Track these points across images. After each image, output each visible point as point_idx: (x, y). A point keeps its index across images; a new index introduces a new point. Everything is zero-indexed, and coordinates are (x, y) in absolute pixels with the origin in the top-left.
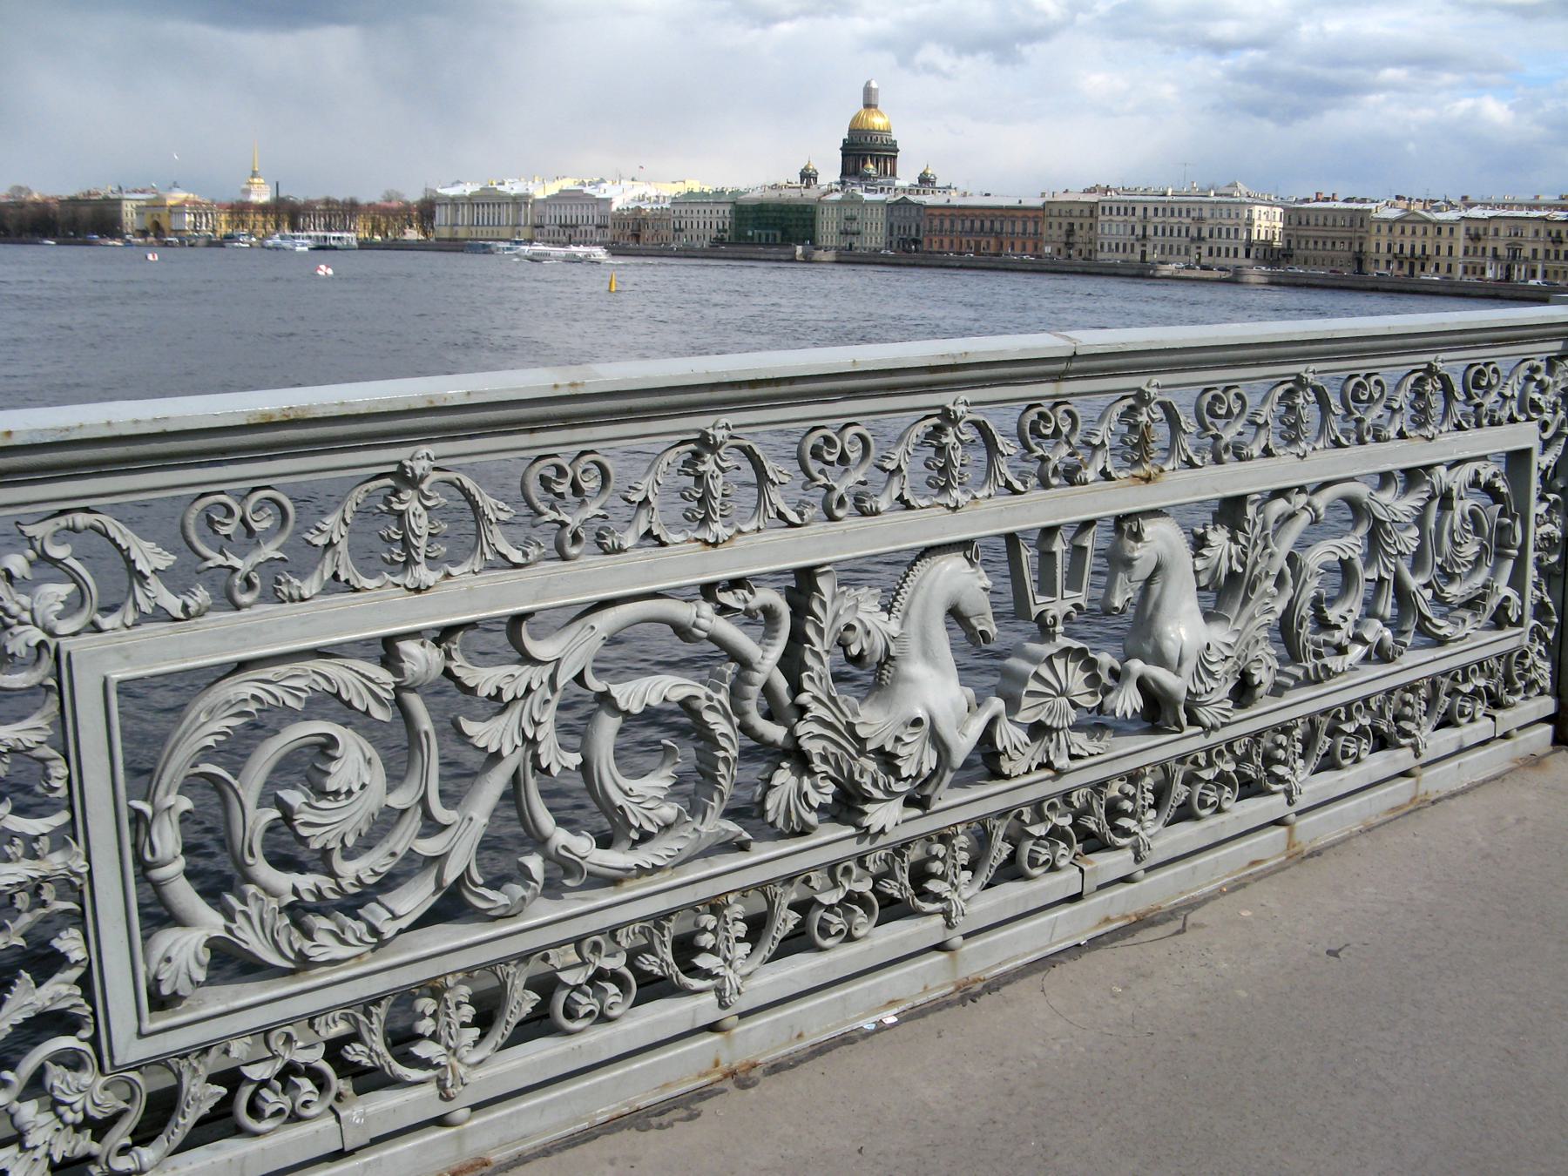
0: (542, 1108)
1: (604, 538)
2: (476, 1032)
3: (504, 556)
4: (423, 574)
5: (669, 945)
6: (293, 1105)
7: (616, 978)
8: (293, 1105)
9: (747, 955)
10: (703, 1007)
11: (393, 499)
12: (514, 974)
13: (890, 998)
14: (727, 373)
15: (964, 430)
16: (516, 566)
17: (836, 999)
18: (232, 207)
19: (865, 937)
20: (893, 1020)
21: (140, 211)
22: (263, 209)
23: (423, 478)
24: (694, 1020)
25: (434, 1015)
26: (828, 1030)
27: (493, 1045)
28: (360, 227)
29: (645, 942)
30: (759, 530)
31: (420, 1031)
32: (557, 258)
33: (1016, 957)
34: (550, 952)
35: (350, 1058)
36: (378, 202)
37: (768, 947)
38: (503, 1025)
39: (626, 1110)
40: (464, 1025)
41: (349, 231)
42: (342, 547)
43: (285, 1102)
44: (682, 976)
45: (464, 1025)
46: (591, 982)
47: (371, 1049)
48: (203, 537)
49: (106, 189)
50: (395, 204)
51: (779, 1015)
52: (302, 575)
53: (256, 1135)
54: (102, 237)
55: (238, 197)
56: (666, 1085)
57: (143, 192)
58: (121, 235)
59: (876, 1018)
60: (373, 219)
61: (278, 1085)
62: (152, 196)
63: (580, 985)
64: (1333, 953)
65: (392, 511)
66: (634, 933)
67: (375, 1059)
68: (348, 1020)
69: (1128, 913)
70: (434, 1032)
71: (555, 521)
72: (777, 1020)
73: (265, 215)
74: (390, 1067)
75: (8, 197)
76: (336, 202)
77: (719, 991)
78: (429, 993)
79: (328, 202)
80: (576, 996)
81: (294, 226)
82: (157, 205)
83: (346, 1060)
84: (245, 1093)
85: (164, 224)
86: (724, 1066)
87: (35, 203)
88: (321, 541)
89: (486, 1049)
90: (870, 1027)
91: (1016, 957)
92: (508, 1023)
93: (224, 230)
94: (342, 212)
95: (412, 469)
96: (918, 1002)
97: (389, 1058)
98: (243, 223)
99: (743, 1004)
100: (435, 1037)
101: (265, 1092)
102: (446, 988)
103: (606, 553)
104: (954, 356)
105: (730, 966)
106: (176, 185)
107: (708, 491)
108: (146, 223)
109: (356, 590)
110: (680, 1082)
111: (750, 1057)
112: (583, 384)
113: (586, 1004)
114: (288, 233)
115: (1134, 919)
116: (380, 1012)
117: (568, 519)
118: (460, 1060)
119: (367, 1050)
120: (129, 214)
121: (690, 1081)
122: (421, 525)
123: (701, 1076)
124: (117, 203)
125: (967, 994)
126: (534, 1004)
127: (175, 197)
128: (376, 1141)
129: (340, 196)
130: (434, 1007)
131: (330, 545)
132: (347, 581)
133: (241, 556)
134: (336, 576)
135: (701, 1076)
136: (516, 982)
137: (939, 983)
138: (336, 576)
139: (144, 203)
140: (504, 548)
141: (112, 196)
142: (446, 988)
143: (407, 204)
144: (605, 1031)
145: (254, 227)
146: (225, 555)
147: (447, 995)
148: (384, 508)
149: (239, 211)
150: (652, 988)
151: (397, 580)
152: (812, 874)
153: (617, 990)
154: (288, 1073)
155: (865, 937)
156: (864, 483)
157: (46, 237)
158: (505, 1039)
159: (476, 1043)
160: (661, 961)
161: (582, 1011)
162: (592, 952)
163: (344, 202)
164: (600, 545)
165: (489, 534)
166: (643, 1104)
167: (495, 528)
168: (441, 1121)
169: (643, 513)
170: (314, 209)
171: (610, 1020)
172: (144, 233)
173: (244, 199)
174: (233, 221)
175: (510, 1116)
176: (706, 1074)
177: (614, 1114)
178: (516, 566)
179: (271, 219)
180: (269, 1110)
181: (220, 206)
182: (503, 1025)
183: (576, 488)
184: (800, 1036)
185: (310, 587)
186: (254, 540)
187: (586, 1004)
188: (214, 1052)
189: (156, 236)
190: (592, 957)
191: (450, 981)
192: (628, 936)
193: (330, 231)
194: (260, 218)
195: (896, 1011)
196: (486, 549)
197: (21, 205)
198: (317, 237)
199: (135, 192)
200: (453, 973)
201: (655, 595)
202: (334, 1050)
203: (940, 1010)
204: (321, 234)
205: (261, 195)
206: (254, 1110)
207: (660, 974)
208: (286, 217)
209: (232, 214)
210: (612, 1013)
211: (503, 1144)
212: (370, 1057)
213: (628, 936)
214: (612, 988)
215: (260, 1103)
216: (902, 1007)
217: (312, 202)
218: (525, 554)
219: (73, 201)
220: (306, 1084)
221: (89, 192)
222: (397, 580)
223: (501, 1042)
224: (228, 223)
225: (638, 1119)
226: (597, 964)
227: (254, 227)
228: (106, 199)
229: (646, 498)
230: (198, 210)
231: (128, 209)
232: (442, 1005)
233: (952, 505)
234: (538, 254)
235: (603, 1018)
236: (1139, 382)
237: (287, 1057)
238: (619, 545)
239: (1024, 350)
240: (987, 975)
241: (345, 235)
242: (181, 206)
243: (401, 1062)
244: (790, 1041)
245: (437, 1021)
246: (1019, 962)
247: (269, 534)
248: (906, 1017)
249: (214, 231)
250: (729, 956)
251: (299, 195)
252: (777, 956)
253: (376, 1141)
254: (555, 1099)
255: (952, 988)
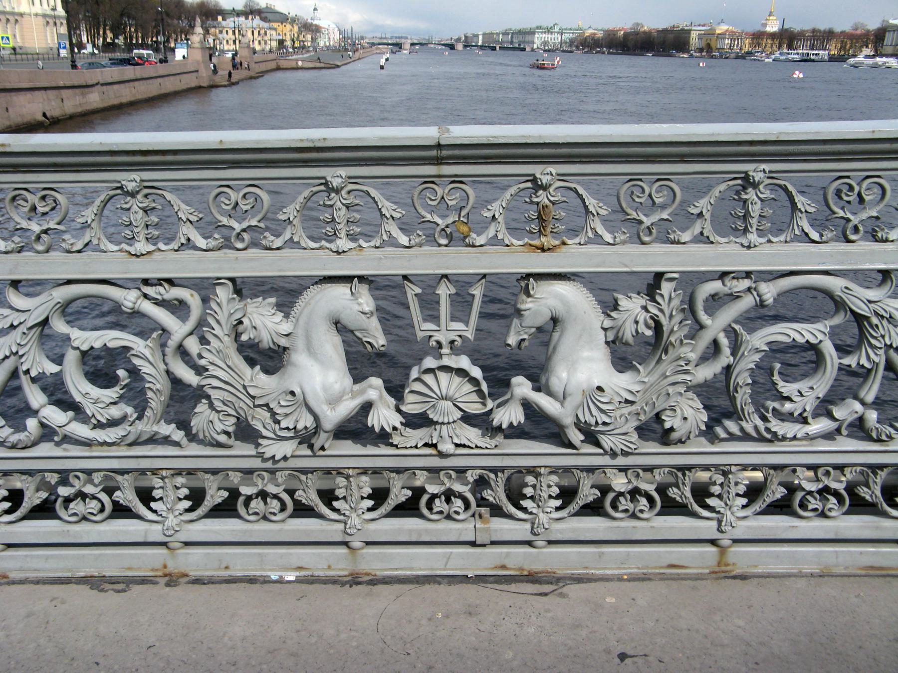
0: (47, 558)
1: (876, 232)
2: (744, 501)
3: (807, 234)
4: (753, 237)
5: (879, 485)
6: (824, 508)
7: (836, 494)
8: (824, 508)
9: (743, 506)
10: (333, 531)
11: (533, 196)
12: (773, 475)
13: (300, 565)
14: (116, 144)
15: (553, 193)
16: (814, 242)
17: (255, 554)
18: (754, 34)
19: (647, 520)
20: (292, 578)
21: (700, 37)
22: (773, 36)
23: (759, 183)
24: (146, 536)
25: (722, 485)
26: (248, 570)
27: (568, 511)
28: (832, 48)
29: (864, 479)
30: (786, 242)
31: (712, 491)
32: (867, 65)
33: (411, 569)
34: (798, 469)
35: (670, 494)
36: (847, 31)
37: (757, 506)
38: (762, 501)
39: (96, 574)
40: (738, 495)
41: (825, 50)
42: (707, 216)
43: (631, 506)
44: (885, 505)
45: (738, 495)
46: (820, 492)
47: (683, 493)
48: (836, 204)
49: (683, 24)
50: (859, 32)
51: (765, 549)
52: (684, 230)
53: (614, 519)
54: (677, 52)
55: (758, 28)
56: (129, 569)
57: (703, 26)
58: (688, 51)
59: (280, 574)
60: (842, 42)
61: (628, 497)
62: (708, 28)
63: (813, 492)
64: (623, 657)
65: (740, 199)
66: (664, 473)
67: (684, 499)
68: (863, 475)
69: (526, 567)
70: (720, 494)
71: (842, 218)
72: (209, 554)
73: (773, 39)
74: (691, 506)
75: (631, 29)
76: (820, 31)
77: (720, 522)
78: (721, 472)
79: (814, 31)
80: (808, 497)
81: (790, 47)
82: (710, 33)
83: (668, 495)
84: (611, 496)
85: (713, 45)
86: (167, 571)
87: (644, 32)
88: (696, 211)
89: (748, 512)
90: (274, 576)
91: (411, 569)
92: (764, 500)
93: (747, 48)
94: (822, 37)
95: (753, 177)
96: (316, 574)
97: (692, 501)
98: (759, 45)
99: (739, 534)
100: (720, 496)
101: (621, 499)
102: (730, 472)
103: (877, 241)
104: (312, 141)
105: (730, 509)
106: (722, 21)
107: (747, 212)
108: (703, 44)
109: (712, 243)
110: (139, 569)
111: (183, 569)
112: (9, 145)
113: (814, 503)
114: (785, 50)
115: (526, 573)
116: (882, 475)
117: (644, 219)
118: (732, 513)
119: (680, 493)
120: (694, 39)
121: (145, 571)
122: (755, 210)
123: (152, 570)
124: (689, 32)
125: (355, 580)
126: (782, 494)
127: (722, 28)
128: (493, 543)
129: (823, 26)
130: (723, 480)
131: (700, 215)
132: (708, 237)
133: (854, 214)
134: (702, 233)
135: (152, 570)
136: (774, 480)
137: (340, 567)
138: (702, 233)
139: (703, 32)
140: (807, 228)
141: (686, 28)
142: (730, 472)
143: (868, 31)
144: (264, 526)
145: (765, 47)
146: (845, 212)
147: (730, 476)
148: (736, 197)
149: (758, 37)
150: (671, 507)
151: (737, 240)
152: (798, 469)
153: (836, 502)
154: (635, 493)
155: (647, 520)
156: (877, 218)
157: (648, 52)
158: (761, 509)
159: (744, 507)
160: (683, 494)
161: (810, 507)
162: (824, 475)
163: (825, 31)
164: (874, 236)
165: (591, 222)
166: (108, 574)
167: (596, 219)
168: (529, 543)
169: (699, 221)
170: (804, 36)
171: (827, 517)
172: (701, 50)
173: (762, 30)
174: (753, 43)
175: (26, 556)
176: (157, 570)
177: (89, 574)
178: (814, 242)
179: (777, 42)
180: (621, 508)
181: (746, 34)
182: (761, 501)
183: (861, 200)
184: (227, 568)
185: (686, 237)
186: (862, 206)
187: (814, 503)
188: (787, 470)
189: (707, 52)
190: (823, 478)
191: (733, 469)
192: (851, 472)
193: (813, 49)
194: (769, 41)
195: (298, 574)
196: (796, 227)
197: (637, 33)
198: (803, 54)
199: (699, 26)
200: (546, 467)
201: (826, 273)
202: (662, 489)
203: (325, 584)
204: (805, 52)
205: (773, 27)
206: (614, 507)
207: (870, 500)
208: (786, 42)
209: (753, 39)
210: (829, 514)
211: (21, 569)
212: (871, 496)
213: (851, 472)
214: (833, 500)
215: (618, 503)
216: (303, 573)
217: (804, 31)
218: (821, 235)
219: (665, 31)
220: (644, 501)
221: (674, 27)
222: (737, 240)
223: (758, 510)
224: (751, 45)
225: (96, 582)
226: (826, 482)
227: (765, 47)
228: (683, 30)
229: (702, 212)
230: (734, 37)
231: (694, 35)
232: (727, 480)
233: (746, 244)
234: (859, 63)
235: (823, 515)
236: (536, 170)
237: (635, 484)
238: (886, 238)
239: (257, 142)
240: (378, 573)
241: (821, 52)
242: (724, 34)
243: (890, 506)
244: (219, 569)
245: (722, 488)
246: (408, 573)
247: (663, 207)
248: (299, 581)
249: (741, 49)
250: (728, 502)
251: (796, 26)
252: (763, 513)
253: (493, 543)
254: (55, 555)
255: (346, 573)
